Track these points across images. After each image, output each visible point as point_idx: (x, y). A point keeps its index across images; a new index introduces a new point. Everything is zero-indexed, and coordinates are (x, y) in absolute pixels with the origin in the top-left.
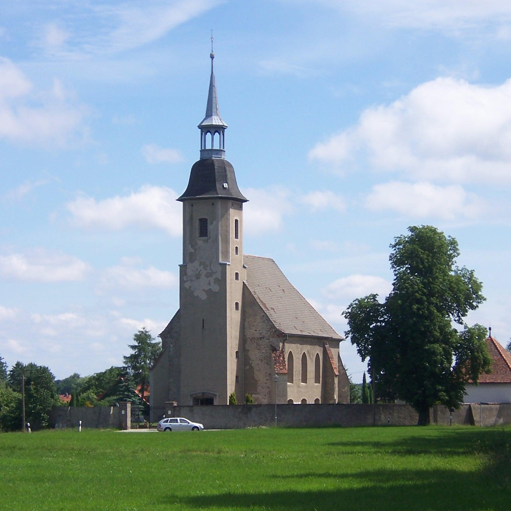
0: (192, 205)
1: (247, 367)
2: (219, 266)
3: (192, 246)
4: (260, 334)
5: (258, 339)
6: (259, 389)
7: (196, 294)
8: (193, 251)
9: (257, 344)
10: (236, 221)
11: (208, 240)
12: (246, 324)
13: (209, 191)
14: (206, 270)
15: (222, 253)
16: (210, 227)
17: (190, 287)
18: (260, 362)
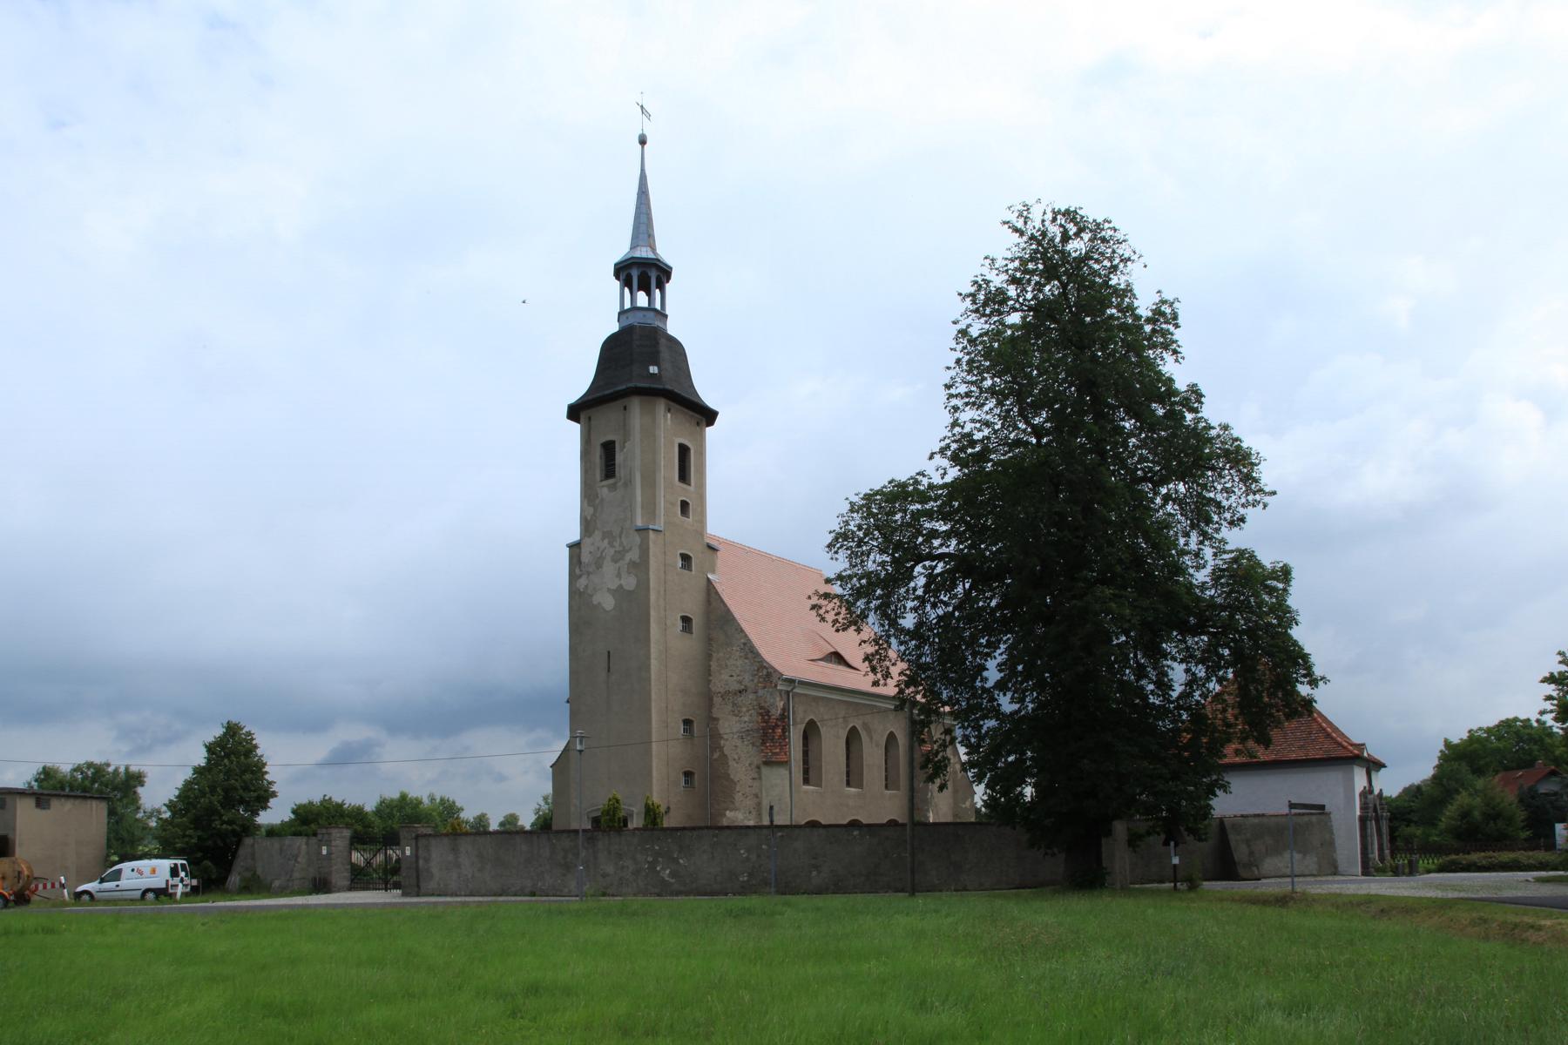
1: (716, 756)
4: (740, 682)
6: (738, 797)
9: (734, 704)
10: (684, 451)
12: (714, 664)
18: (739, 743)
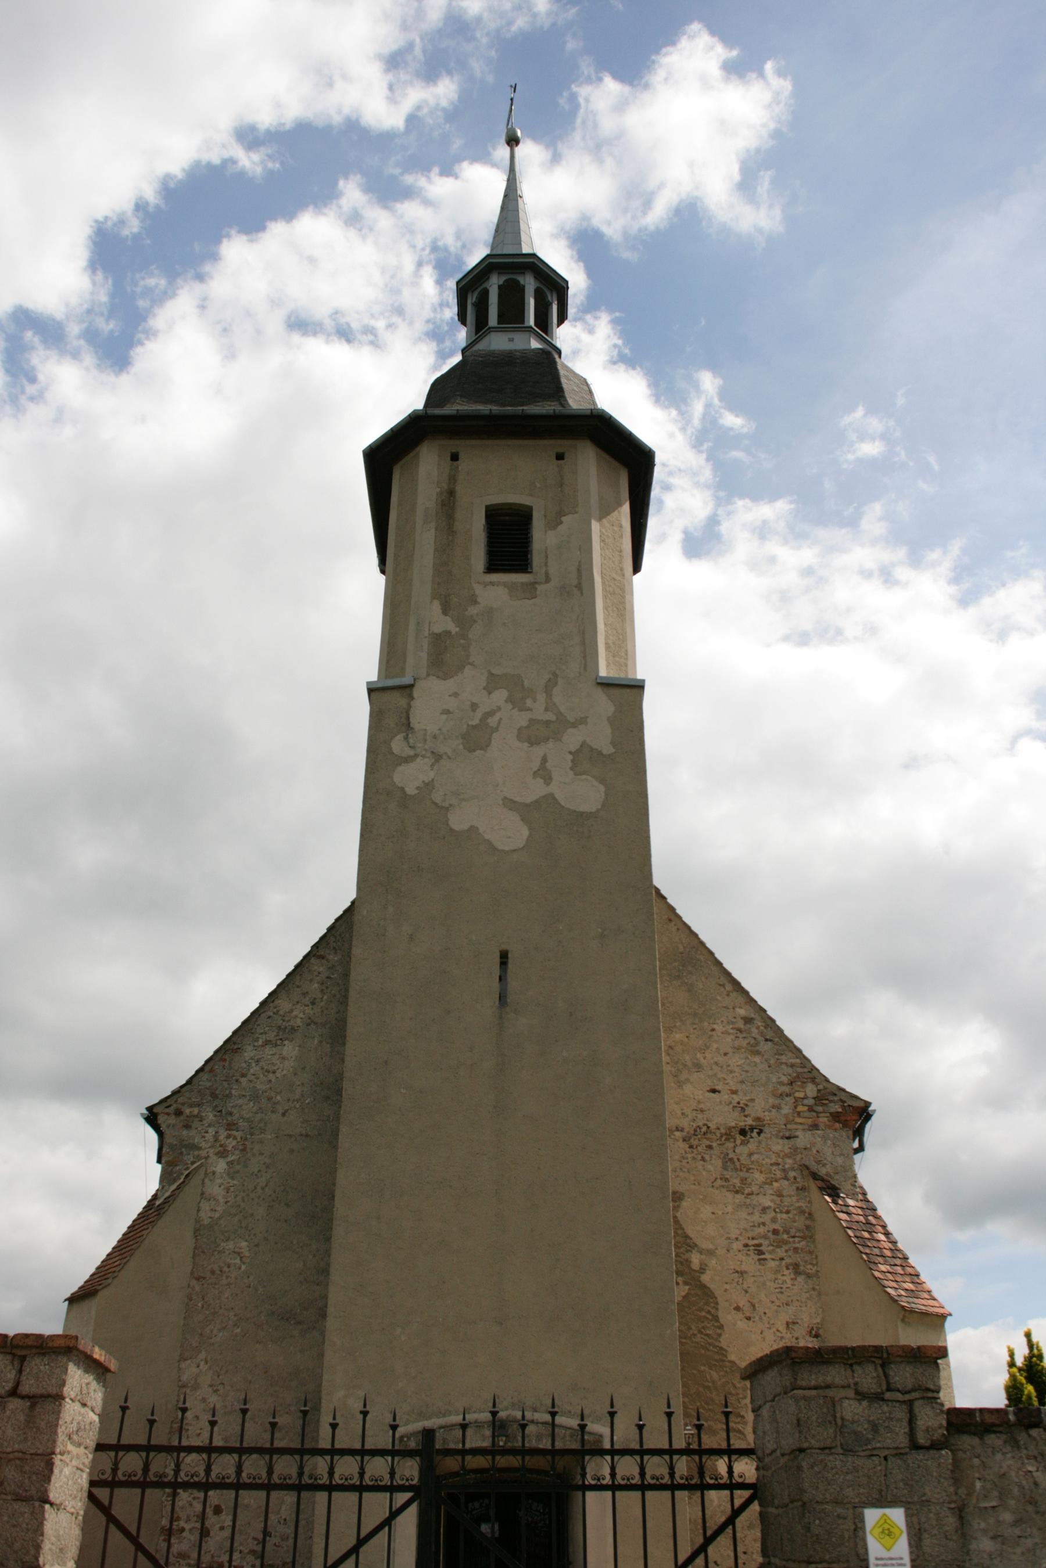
0: (455, 457)
2: (600, 694)
3: (445, 611)
5: (728, 1135)
7: (458, 821)
8: (453, 629)
9: (728, 1161)
11: (533, 585)
13: (502, 463)
14: (523, 709)
15: (608, 647)
16: (543, 539)
17: (429, 786)
18: (749, 1263)
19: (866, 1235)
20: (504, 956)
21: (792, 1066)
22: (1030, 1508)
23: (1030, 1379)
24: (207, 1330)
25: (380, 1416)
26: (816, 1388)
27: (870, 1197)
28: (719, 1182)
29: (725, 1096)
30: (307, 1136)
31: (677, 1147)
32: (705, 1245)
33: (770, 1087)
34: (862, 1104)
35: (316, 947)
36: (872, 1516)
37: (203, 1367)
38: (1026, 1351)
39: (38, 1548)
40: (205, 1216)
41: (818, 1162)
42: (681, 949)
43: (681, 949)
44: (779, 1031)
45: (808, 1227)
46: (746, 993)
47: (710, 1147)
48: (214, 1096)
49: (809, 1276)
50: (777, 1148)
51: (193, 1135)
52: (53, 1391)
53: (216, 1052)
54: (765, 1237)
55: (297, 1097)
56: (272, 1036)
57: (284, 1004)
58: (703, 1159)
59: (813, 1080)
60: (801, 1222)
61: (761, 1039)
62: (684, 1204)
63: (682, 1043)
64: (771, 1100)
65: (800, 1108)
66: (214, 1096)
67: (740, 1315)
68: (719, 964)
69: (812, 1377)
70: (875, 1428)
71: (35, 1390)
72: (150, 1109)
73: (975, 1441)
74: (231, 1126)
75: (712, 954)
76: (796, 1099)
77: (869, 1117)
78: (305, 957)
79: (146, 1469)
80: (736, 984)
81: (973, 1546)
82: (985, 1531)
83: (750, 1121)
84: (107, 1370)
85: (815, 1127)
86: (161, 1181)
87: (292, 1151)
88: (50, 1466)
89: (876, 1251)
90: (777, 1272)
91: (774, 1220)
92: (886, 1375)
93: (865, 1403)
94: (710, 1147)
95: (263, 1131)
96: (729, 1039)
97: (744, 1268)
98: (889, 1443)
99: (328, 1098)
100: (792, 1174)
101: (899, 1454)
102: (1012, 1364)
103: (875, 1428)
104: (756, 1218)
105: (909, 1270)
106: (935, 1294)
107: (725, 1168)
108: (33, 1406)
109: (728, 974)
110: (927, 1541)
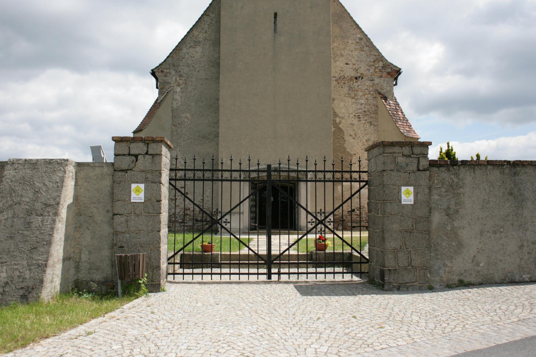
5: (351, 79)
9: (350, 88)
18: (355, 121)
19: (395, 113)
20: (276, 14)
21: (375, 55)
22: (450, 188)
23: (447, 157)
24: (179, 141)
25: (254, 162)
26: (390, 153)
27: (397, 101)
28: (347, 95)
29: (351, 66)
30: (207, 79)
31: (334, 83)
32: (341, 115)
33: (367, 63)
34: (398, 69)
35: (206, 11)
36: (404, 189)
37: (179, 152)
38: (447, 148)
39: (160, 195)
40: (175, 105)
41: (381, 89)
42: (338, 12)
43: (338, 12)
44: (372, 43)
45: (376, 110)
46: (360, 29)
47: (345, 83)
48: (174, 65)
49: (375, 126)
50: (367, 84)
51: (168, 79)
52: (159, 153)
53: (173, 50)
54: (361, 113)
55: (203, 66)
56: (192, 44)
57: (195, 33)
58: (342, 87)
59: (382, 61)
60: (374, 108)
61: (365, 46)
62: (335, 102)
63: (337, 47)
64: (367, 68)
65: (377, 70)
66: (174, 65)
67: (351, 137)
68: (351, 18)
69: (389, 150)
70: (407, 165)
71: (153, 153)
72: (152, 70)
73: (437, 169)
74: (180, 76)
75: (349, 14)
76: (375, 67)
77: (400, 74)
78: (202, 15)
79: (185, 176)
80: (357, 25)
81: (432, 197)
82: (436, 194)
83: (359, 75)
84: (171, 148)
85: (381, 77)
86: (159, 94)
87: (202, 84)
88: (160, 173)
89: (398, 118)
90: (364, 124)
91: (365, 108)
92: (412, 150)
93: (405, 158)
94: (345, 83)
95: (192, 77)
96: (354, 45)
97: (353, 123)
98: (411, 169)
99: (213, 66)
100: (372, 93)
101: (414, 172)
102: (441, 152)
103: (407, 165)
104: (359, 107)
105: (408, 124)
106: (416, 132)
107: (349, 90)
108: (153, 157)
109: (354, 22)
110: (419, 195)
